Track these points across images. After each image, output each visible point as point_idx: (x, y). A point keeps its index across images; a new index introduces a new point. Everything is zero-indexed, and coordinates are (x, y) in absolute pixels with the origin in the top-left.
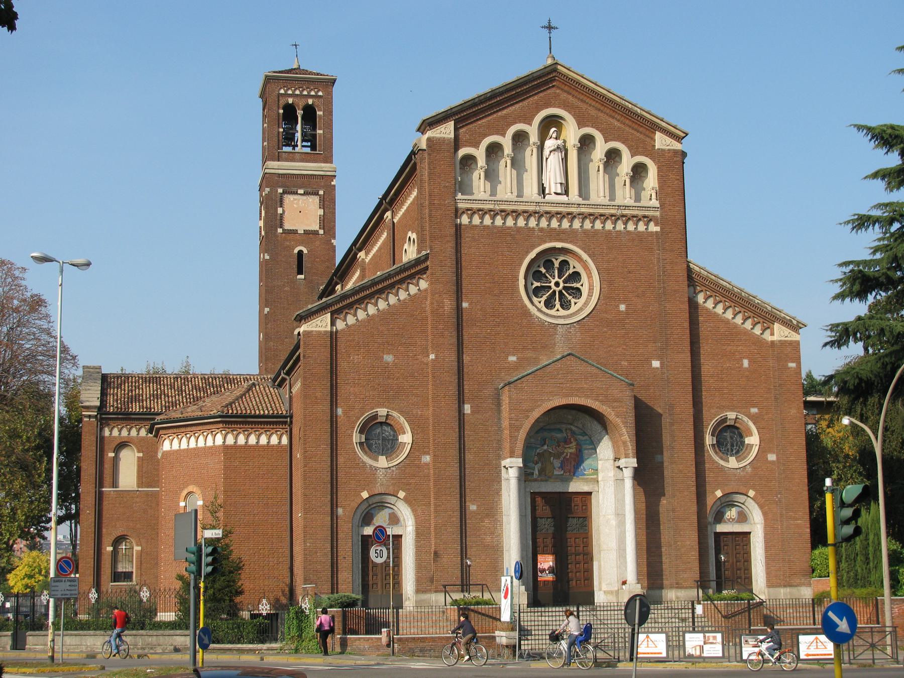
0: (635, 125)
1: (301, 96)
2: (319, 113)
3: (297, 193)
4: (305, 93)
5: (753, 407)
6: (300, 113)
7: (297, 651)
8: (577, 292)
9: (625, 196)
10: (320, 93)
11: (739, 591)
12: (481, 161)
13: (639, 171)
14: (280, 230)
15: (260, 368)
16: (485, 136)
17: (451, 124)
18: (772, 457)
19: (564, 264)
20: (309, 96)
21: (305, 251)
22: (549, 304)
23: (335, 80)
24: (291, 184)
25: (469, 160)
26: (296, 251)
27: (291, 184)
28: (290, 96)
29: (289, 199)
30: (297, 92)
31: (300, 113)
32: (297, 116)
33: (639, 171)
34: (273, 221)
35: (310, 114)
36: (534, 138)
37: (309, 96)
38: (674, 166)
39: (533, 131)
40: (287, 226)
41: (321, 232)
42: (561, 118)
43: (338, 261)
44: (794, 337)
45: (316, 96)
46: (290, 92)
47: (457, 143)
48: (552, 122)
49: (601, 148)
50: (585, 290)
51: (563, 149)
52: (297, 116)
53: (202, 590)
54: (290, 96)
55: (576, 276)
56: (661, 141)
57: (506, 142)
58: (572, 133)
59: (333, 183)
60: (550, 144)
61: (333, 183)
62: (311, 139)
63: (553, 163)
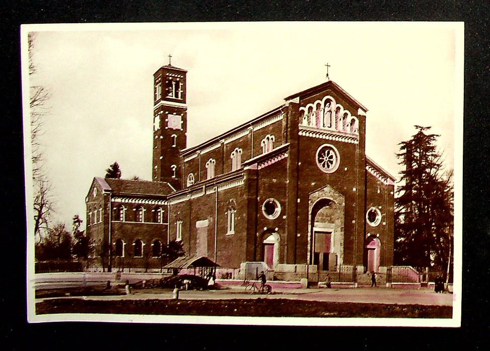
0: (352, 106)
4: (176, 76)
5: (297, 200)
7: (146, 272)
8: (332, 163)
9: (348, 129)
12: (306, 113)
13: (353, 121)
15: (154, 174)
17: (298, 98)
18: (384, 223)
19: (329, 153)
20: (177, 77)
22: (328, 166)
24: (172, 110)
25: (303, 111)
27: (172, 110)
28: (170, 76)
29: (170, 116)
30: (173, 75)
33: (353, 121)
34: (163, 123)
36: (322, 106)
38: (362, 120)
39: (322, 103)
41: (167, 128)
42: (332, 101)
44: (393, 184)
46: (170, 75)
47: (299, 105)
48: (328, 101)
49: (342, 111)
50: (334, 163)
51: (330, 111)
54: (170, 76)
55: (331, 157)
56: (360, 112)
57: (314, 106)
58: (334, 105)
60: (327, 109)
63: (327, 115)
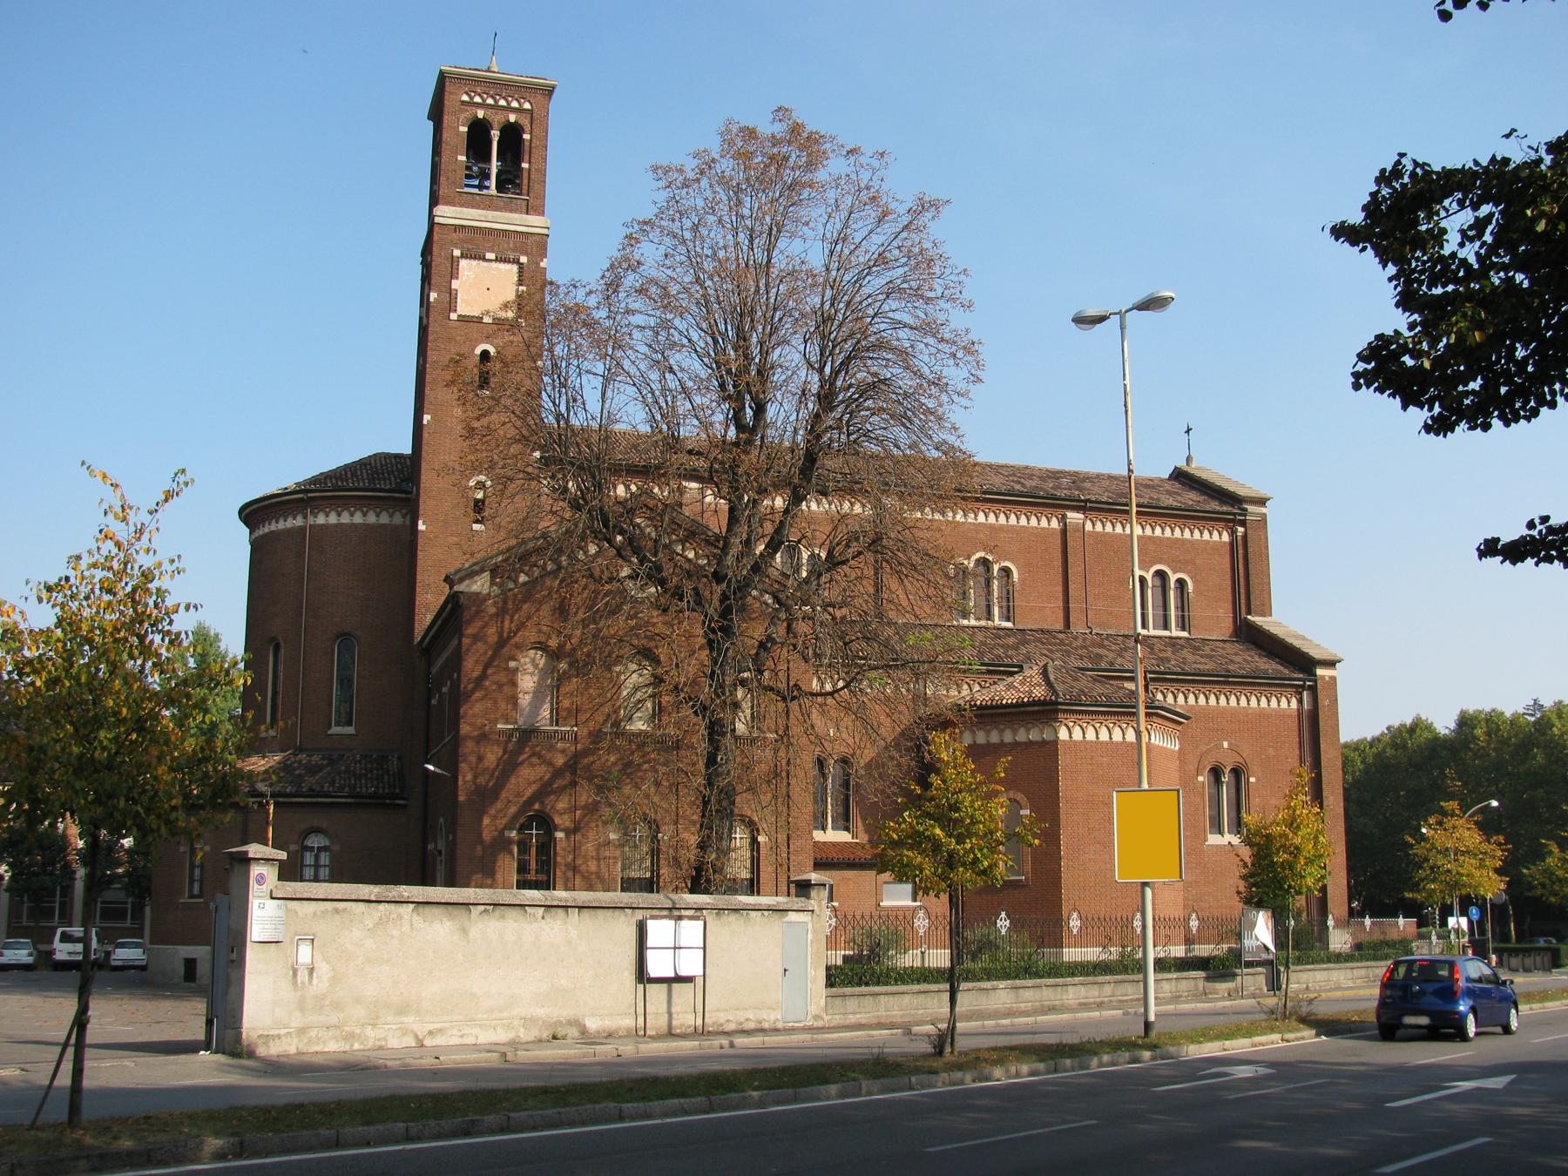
1: (496, 107)
2: (526, 137)
3: (484, 259)
6: (495, 135)
10: (527, 106)
11: (732, 1045)
14: (457, 253)
16: (1188, 573)
21: (492, 350)
23: (554, 87)
24: (477, 244)
26: (478, 351)
31: (495, 135)
32: (492, 148)
35: (512, 134)
37: (509, 109)
40: (463, 263)
43: (418, 639)
45: (519, 111)
52: (492, 148)
53: (79, 886)
59: (542, 265)
61: (542, 265)
62: (510, 180)
